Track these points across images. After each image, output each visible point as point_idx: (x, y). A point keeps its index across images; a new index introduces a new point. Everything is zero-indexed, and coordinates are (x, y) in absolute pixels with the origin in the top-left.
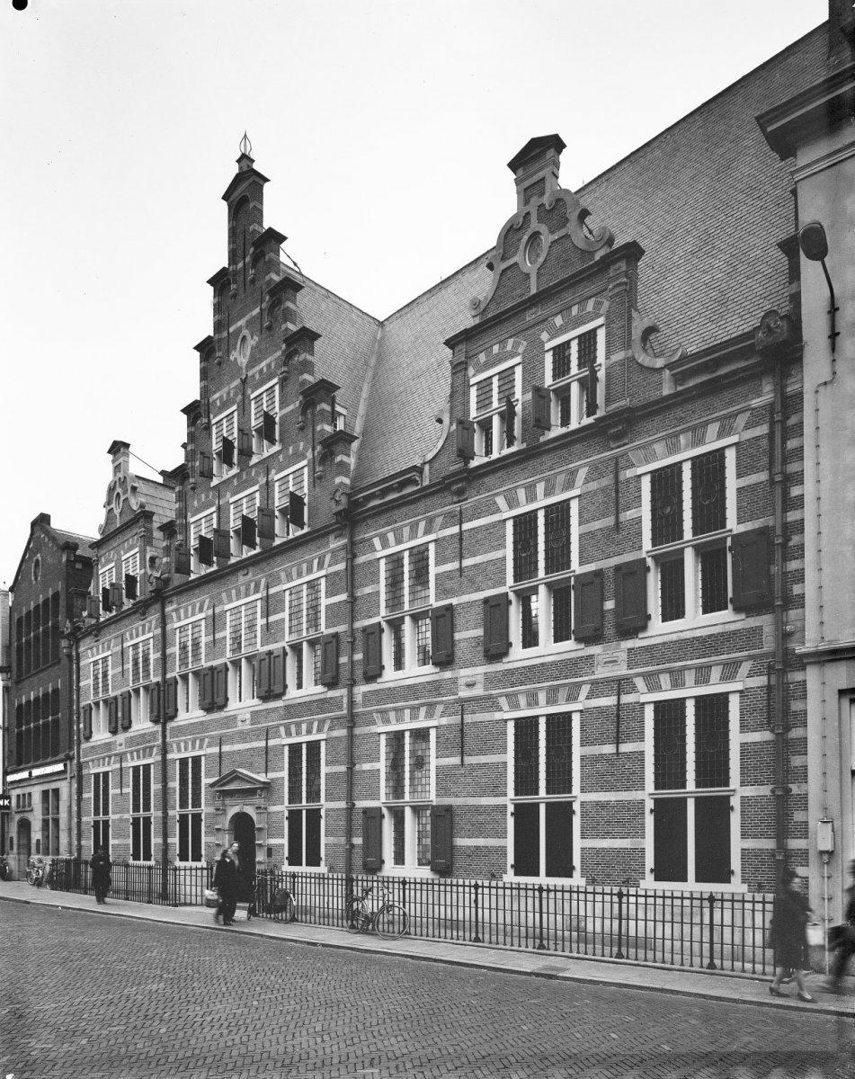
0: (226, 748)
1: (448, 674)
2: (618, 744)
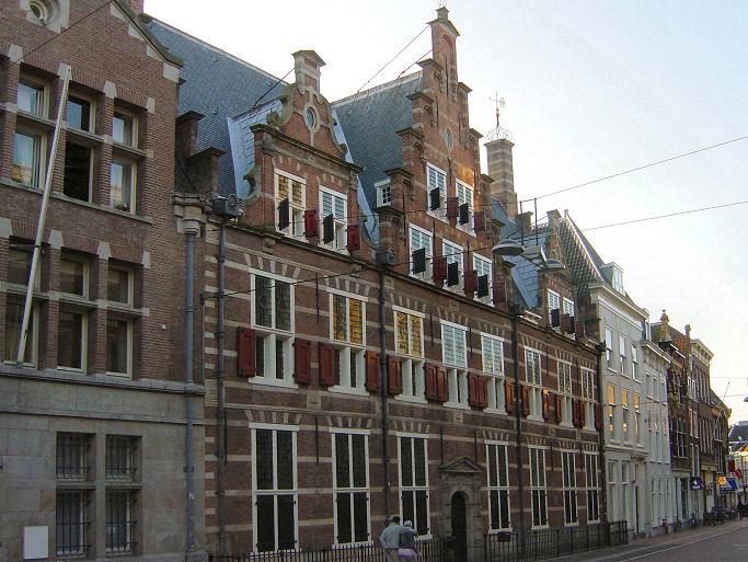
0: (445, 437)
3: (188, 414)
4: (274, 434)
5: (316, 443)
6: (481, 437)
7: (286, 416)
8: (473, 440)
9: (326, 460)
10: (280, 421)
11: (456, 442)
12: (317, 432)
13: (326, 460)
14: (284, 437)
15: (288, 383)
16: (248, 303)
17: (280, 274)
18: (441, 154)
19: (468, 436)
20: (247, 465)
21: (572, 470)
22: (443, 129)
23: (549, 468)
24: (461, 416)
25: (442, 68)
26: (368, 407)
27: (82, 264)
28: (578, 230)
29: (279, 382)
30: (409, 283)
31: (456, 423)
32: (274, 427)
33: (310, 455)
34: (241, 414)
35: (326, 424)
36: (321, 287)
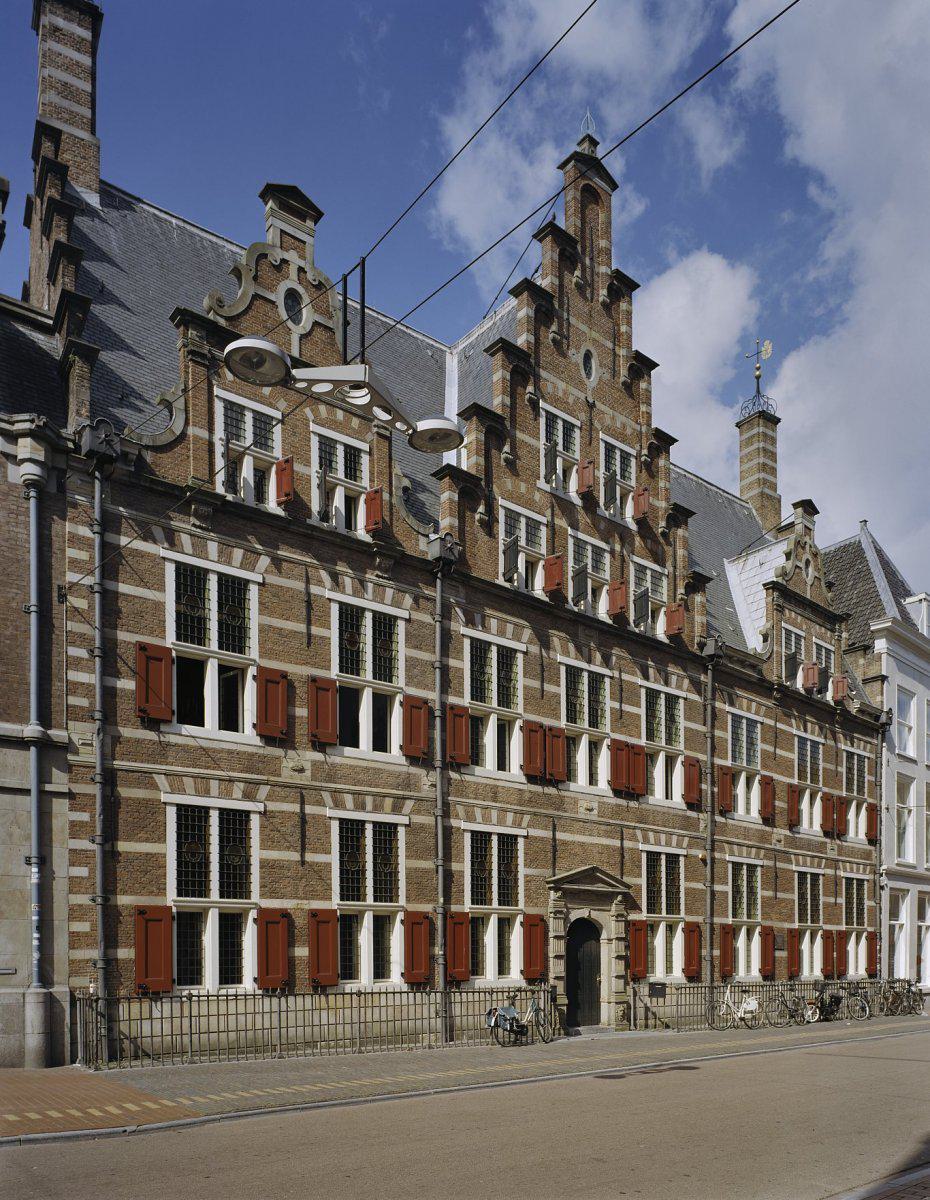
1: (767, 829)
2: (303, 850)
3: (43, 777)
4: (369, 828)
5: (304, 832)
6: (634, 838)
7: (389, 802)
8: (617, 843)
9: (320, 858)
10: (377, 808)
11: (582, 845)
12: (303, 817)
13: (320, 858)
14: (508, 842)
15: (247, 735)
16: (160, 607)
17: (229, 563)
18: (572, 389)
19: (608, 835)
20: (158, 861)
21: (802, 896)
22: (578, 348)
23: (770, 893)
24: (595, 805)
25: (576, 242)
26: (408, 783)
27: (60, 588)
28: (879, 552)
29: (668, 803)
30: (496, 596)
31: (582, 814)
32: (214, 802)
33: (544, 867)
34: (146, 779)
35: (321, 803)
36: (314, 589)
